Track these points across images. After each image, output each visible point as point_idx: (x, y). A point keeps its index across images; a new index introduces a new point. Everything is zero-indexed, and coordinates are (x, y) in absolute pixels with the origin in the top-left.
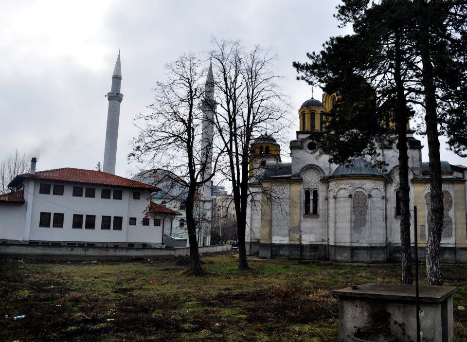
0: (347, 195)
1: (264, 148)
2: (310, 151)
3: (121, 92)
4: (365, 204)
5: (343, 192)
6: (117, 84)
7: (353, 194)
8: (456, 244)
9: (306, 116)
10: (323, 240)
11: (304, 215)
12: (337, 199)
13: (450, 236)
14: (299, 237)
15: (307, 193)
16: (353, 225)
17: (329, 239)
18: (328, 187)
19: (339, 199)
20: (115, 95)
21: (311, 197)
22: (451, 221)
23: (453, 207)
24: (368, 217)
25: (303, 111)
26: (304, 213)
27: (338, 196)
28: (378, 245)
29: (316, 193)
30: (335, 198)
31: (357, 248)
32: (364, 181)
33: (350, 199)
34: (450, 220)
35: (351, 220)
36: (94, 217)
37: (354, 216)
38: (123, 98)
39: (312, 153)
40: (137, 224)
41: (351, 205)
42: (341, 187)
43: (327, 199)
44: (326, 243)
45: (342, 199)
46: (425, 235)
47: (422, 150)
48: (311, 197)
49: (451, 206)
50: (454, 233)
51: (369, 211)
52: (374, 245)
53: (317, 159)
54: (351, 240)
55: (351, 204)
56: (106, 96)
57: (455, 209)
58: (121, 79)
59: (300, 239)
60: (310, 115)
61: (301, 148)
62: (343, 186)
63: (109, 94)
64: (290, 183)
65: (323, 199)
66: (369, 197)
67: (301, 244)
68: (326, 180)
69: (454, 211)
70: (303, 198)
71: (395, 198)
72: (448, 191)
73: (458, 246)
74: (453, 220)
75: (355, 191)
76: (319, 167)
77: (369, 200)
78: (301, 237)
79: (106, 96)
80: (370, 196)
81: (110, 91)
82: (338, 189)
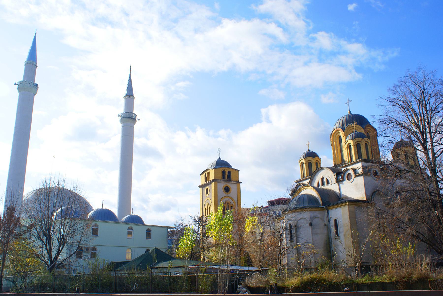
1: (227, 174)
58: (37, 67)
79: (15, 84)
81: (21, 79)
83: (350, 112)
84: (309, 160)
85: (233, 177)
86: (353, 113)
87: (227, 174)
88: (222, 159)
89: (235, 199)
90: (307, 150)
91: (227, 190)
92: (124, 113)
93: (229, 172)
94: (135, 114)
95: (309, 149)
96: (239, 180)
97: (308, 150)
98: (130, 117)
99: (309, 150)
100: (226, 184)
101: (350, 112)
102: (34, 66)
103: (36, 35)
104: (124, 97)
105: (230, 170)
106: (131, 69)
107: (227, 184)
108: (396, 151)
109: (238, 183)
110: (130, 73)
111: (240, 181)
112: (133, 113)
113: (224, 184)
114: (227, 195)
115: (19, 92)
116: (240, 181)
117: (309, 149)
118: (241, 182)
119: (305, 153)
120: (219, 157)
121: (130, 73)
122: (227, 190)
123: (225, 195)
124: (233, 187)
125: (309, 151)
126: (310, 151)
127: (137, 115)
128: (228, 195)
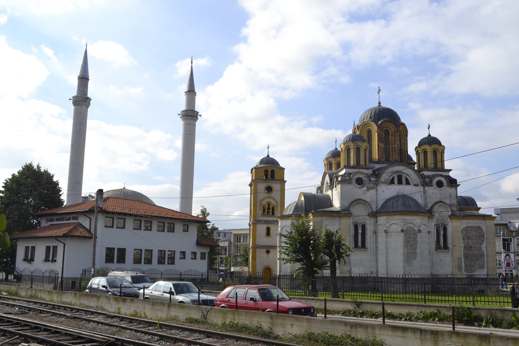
0: (399, 229)
1: (269, 173)
2: (359, 186)
3: (89, 95)
4: (415, 239)
5: (394, 227)
6: (85, 86)
7: (405, 229)
8: (488, 275)
9: (352, 151)
10: (372, 273)
11: (354, 248)
12: (388, 234)
13: (482, 267)
14: (349, 269)
15: (356, 227)
16: (405, 258)
17: (378, 272)
18: (377, 222)
19: (391, 233)
20: (83, 100)
21: (360, 231)
22: (483, 254)
23: (485, 240)
24: (418, 251)
25: (348, 146)
26: (354, 247)
27: (389, 231)
28: (426, 277)
29: (364, 227)
30: (386, 232)
31: (408, 279)
32: (415, 217)
33: (402, 234)
34: (483, 253)
35: (404, 253)
36: (151, 251)
37: (406, 250)
38: (91, 102)
39: (360, 188)
40: (197, 258)
41: (403, 240)
42: (392, 222)
43: (375, 233)
44: (375, 275)
45: (393, 234)
46: (462, 267)
47: (458, 188)
48: (360, 231)
49: (483, 241)
50: (486, 265)
51: (418, 245)
52: (423, 277)
53: (364, 194)
54: (404, 272)
55: (403, 238)
56: (70, 99)
57: (486, 243)
58: (88, 80)
59: (350, 271)
60: (355, 149)
61: (350, 183)
62: (395, 222)
63: (73, 97)
64: (340, 217)
65: (371, 233)
66: (419, 232)
67: (351, 276)
68: (375, 215)
69: (485, 244)
70: (353, 232)
71: (436, 233)
72: (480, 227)
73: (489, 277)
74: (485, 254)
75: (407, 226)
76: (366, 202)
77: (419, 235)
78: (351, 269)
79: (70, 99)
80: (420, 231)
81: (75, 94)
82: (389, 225)
83: (380, 103)
84: (425, 148)
85: (277, 176)
86: (384, 105)
87: (269, 173)
88: (432, 135)
89: (278, 199)
90: (334, 149)
91: (269, 189)
92: (185, 110)
93: (273, 171)
94: (196, 111)
95: (336, 148)
96: (284, 179)
97: (335, 148)
98: (189, 114)
99: (268, 156)
100: (268, 184)
101: (380, 103)
102: (85, 79)
103: (86, 48)
104: (185, 92)
105: (275, 169)
106: (192, 61)
107: (270, 184)
108: (38, 190)
109: (283, 182)
110: (192, 66)
111: (285, 180)
112: (195, 111)
113: (266, 184)
114: (268, 195)
115: (74, 106)
116: (285, 180)
117: (336, 148)
118: (286, 181)
119: (332, 152)
120: (268, 155)
121: (192, 66)
122: (269, 189)
123: (267, 195)
124: (276, 187)
125: (335, 149)
126: (337, 149)
127: (198, 111)
128: (270, 195)
